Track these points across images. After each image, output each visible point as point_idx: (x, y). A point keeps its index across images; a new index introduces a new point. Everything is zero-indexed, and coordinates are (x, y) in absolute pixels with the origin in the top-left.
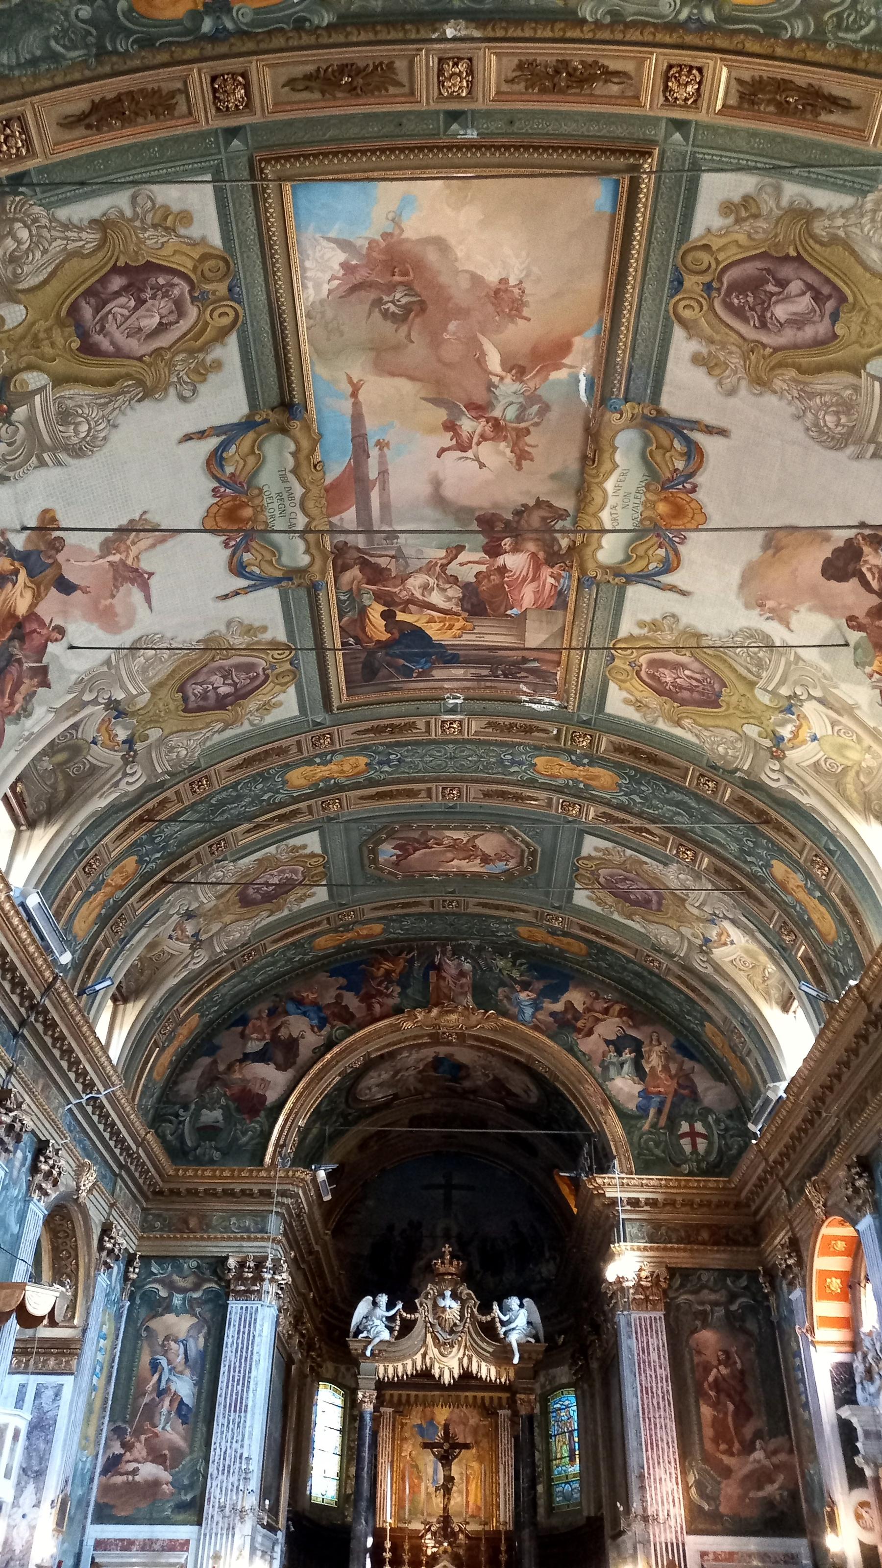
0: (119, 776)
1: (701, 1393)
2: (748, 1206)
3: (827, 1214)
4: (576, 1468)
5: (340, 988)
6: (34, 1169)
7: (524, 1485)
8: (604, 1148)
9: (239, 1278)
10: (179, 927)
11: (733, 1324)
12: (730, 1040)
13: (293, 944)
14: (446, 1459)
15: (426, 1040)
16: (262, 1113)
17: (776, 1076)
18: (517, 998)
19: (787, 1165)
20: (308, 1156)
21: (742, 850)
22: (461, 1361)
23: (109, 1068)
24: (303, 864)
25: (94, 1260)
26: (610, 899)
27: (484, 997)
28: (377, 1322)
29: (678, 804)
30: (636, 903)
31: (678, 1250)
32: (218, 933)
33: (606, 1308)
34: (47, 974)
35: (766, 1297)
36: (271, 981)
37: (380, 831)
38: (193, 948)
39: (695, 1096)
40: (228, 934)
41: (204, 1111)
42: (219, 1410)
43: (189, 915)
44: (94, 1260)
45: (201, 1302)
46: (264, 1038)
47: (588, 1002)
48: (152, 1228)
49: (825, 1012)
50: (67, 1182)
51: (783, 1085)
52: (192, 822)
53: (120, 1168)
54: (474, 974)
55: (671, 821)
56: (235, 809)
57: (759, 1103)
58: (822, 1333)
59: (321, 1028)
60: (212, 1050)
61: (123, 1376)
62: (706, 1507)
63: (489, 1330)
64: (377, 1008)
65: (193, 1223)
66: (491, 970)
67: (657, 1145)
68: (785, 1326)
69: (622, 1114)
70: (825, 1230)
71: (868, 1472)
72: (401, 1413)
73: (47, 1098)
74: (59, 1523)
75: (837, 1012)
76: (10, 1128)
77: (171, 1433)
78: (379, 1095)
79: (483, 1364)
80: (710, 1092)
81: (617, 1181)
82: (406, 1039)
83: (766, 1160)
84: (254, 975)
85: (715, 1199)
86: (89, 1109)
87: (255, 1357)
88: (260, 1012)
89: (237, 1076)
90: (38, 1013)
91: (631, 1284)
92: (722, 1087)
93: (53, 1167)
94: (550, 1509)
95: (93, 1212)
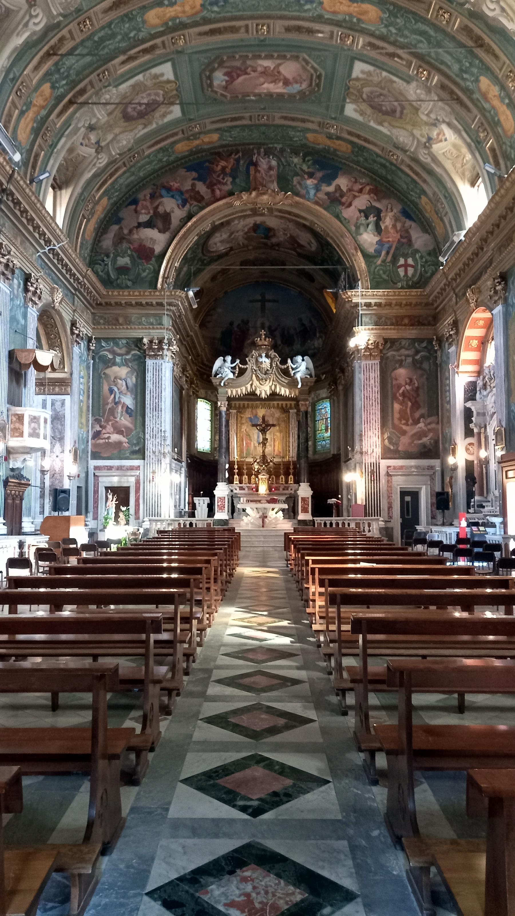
0: (27, 17)
1: (395, 398)
2: (432, 304)
3: (477, 306)
4: (329, 434)
5: (194, 179)
6: (26, 290)
7: (302, 441)
8: (353, 275)
9: (150, 348)
10: (86, 137)
11: (416, 365)
12: (436, 206)
13: (161, 149)
14: (263, 431)
15: (249, 213)
16: (153, 259)
17: (460, 228)
18: (305, 184)
19: (458, 280)
20: (182, 283)
21: (461, 70)
22: (271, 387)
23: (58, 231)
24: (161, 87)
25: (69, 341)
26: (369, 111)
27: (285, 184)
28: (226, 370)
29: (422, 33)
30: (386, 113)
31: (390, 329)
32: (112, 141)
33: (348, 360)
34: (8, 168)
35: (436, 351)
36: (150, 175)
37: (213, 61)
38: (97, 152)
39: (410, 243)
40: (118, 142)
41: (119, 258)
42: (147, 411)
43: (91, 128)
44: (69, 341)
45: (130, 360)
46: (149, 213)
47: (350, 185)
48: (99, 324)
49: (498, 185)
50: (46, 297)
51: (464, 232)
52: (84, 56)
53: (75, 290)
54: (278, 169)
55: (415, 47)
56: (111, 45)
57: (448, 244)
58: (463, 368)
59: (183, 206)
60: (119, 221)
61: (95, 396)
62: (392, 448)
63: (286, 373)
64: (218, 192)
65: (121, 320)
66: (289, 165)
67: (384, 273)
68: (443, 365)
69: (366, 255)
70: (474, 315)
71: (476, 430)
72: (240, 412)
73: (25, 249)
74: (75, 459)
75: (504, 183)
76: (7, 266)
77: (125, 421)
78: (222, 248)
79: (282, 388)
80: (420, 240)
81: (360, 293)
82: (237, 212)
83: (447, 279)
84: (139, 171)
85: (414, 302)
86: (51, 256)
87: (163, 386)
88: (145, 196)
89: (135, 236)
90: (7, 195)
91: (363, 347)
92: (426, 237)
93: (36, 288)
94: (315, 452)
95: (64, 314)
